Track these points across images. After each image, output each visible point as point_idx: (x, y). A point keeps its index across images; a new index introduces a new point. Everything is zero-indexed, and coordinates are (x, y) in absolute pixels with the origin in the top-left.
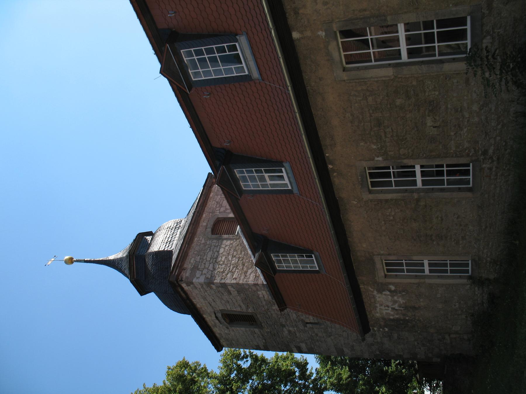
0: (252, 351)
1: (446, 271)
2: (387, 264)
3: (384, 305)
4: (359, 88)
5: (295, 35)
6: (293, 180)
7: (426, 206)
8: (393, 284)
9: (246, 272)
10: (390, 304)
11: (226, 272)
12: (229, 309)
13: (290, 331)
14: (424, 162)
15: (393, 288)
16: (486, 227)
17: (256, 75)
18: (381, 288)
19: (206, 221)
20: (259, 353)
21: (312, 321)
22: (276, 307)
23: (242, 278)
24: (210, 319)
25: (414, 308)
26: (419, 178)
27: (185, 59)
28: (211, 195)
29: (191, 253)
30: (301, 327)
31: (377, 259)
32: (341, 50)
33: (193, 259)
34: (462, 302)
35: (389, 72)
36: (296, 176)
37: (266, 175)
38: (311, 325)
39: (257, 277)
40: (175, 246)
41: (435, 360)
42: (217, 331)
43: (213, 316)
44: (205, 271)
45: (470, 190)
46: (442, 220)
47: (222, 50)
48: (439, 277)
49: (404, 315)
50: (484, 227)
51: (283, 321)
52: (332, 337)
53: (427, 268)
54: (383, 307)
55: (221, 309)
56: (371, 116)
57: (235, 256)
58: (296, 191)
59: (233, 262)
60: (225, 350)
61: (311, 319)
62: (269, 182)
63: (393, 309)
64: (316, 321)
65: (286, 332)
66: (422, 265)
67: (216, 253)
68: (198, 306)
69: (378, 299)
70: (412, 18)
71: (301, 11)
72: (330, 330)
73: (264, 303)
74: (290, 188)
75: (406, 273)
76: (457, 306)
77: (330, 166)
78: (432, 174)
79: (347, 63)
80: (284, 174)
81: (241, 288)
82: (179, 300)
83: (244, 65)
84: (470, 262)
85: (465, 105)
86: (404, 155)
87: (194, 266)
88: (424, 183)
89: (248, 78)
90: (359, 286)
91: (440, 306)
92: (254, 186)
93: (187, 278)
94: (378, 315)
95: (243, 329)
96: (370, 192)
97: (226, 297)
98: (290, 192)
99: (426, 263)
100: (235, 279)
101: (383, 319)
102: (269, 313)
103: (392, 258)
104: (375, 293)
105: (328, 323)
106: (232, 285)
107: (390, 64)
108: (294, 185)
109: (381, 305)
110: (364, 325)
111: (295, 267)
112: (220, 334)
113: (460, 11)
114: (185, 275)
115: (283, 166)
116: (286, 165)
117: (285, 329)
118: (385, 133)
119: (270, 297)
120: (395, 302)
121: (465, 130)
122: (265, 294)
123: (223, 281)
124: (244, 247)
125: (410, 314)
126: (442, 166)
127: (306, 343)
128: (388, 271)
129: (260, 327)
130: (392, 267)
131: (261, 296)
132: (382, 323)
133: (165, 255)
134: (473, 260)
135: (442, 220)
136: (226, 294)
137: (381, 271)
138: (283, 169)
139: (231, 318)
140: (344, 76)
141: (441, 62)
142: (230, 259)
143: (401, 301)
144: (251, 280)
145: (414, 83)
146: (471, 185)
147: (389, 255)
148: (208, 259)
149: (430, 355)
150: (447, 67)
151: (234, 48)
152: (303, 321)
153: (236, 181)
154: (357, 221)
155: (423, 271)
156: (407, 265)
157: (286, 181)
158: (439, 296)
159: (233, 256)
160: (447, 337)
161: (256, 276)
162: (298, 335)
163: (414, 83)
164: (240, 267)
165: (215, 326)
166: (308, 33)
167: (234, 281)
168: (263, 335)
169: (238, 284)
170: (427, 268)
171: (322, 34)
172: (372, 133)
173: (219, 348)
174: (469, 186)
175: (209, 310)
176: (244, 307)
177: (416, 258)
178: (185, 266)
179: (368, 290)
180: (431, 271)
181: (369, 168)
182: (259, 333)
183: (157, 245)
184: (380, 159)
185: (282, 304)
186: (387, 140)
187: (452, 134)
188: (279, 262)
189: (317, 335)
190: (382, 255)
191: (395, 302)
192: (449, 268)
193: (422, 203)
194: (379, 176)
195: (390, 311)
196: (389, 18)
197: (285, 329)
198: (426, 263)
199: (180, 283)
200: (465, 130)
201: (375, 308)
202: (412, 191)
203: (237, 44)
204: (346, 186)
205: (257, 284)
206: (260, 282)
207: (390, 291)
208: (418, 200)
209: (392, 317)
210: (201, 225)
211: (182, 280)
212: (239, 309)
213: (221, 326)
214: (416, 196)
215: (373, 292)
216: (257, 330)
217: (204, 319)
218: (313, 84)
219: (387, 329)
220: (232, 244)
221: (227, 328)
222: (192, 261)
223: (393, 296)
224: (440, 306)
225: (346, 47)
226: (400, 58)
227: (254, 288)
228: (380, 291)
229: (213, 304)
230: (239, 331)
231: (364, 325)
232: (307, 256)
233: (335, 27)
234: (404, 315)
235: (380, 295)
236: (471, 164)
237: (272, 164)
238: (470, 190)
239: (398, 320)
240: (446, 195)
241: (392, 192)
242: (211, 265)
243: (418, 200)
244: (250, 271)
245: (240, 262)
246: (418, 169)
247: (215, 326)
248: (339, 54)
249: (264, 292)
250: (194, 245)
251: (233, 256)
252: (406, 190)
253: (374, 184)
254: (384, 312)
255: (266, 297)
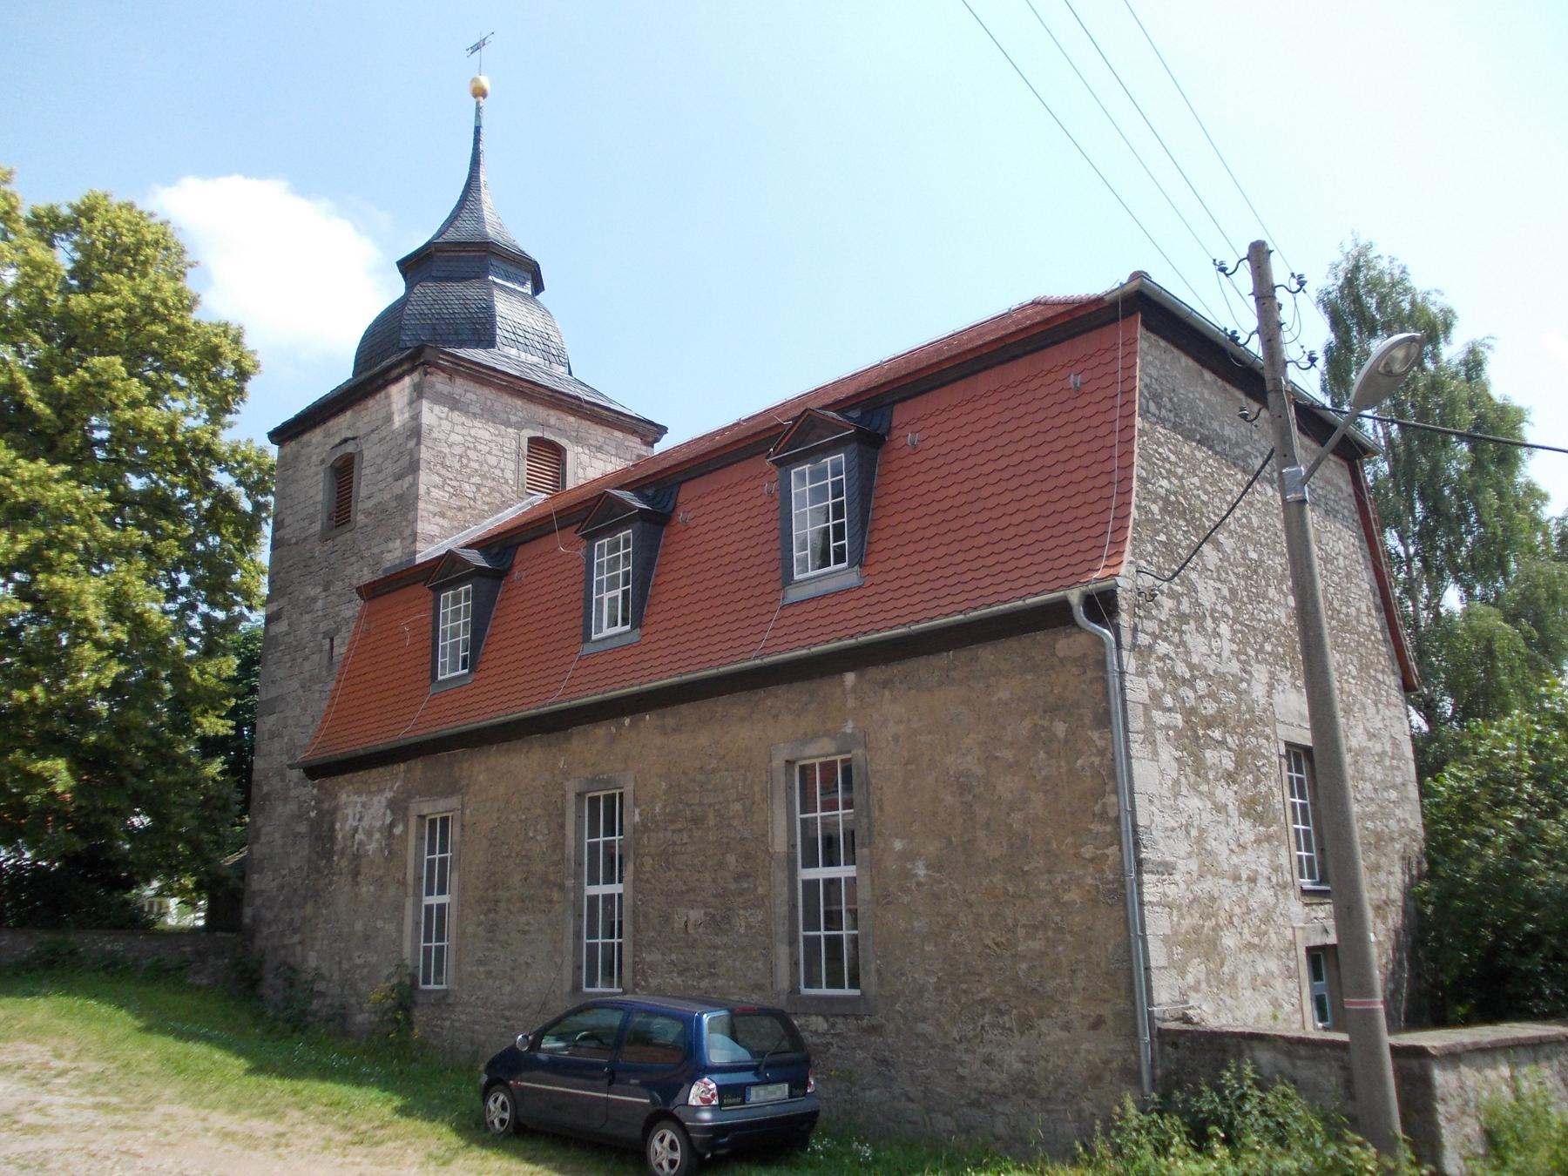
0: (270, 521)
1: (428, 939)
2: (445, 821)
3: (363, 810)
4: (756, 789)
5: (850, 678)
6: (609, 645)
7: (551, 902)
8: (406, 831)
9: (443, 516)
10: (365, 823)
11: (443, 472)
12: (364, 472)
13: (314, 600)
14: (627, 902)
15: (398, 831)
16: (507, 1019)
17: (794, 594)
18: (398, 807)
19: (556, 426)
20: (267, 530)
21: (336, 650)
22: (367, 576)
23: (431, 507)
24: (342, 425)
25: (356, 874)
26: (601, 890)
27: (828, 460)
28: (618, 434)
29: (487, 393)
30: (323, 627)
31: (454, 801)
32: (823, 760)
33: (474, 398)
34: (365, 971)
35: (780, 846)
36: (614, 649)
37: (619, 593)
38: (327, 647)
39: (431, 539)
40: (506, 357)
41: (248, 912)
42: (316, 436)
43: (350, 435)
44: (446, 425)
45: (577, 987)
46: (525, 932)
47: (839, 535)
48: (418, 924)
49: (343, 853)
50: (507, 1013)
51: (338, 586)
52: (300, 692)
53: (435, 900)
54: (359, 808)
55: (365, 453)
56: (710, 805)
57: (478, 490)
58: (588, 649)
59: (466, 486)
60: (273, 451)
61: (340, 650)
62: (606, 596)
63: (356, 830)
64: (335, 659)
65: (312, 592)
66: (442, 891)
67: (485, 449)
68: (371, 403)
69: (375, 799)
70: (864, 893)
71: (887, 693)
72: (317, 687)
73: (376, 550)
74: (594, 637)
75: (427, 857)
76: (358, 961)
77: (627, 721)
78: (607, 915)
79: (803, 768)
80: (619, 629)
81: (407, 503)
82: (392, 352)
83: (811, 574)
84: (444, 987)
85: (720, 982)
86: (642, 864)
87: (458, 401)
88: (593, 900)
89: (787, 579)
90: (404, 761)
91: (359, 926)
92: (600, 565)
93: (432, 386)
94: (343, 797)
95: (320, 497)
96: (580, 796)
97: (390, 468)
98: (587, 637)
99: (444, 899)
100: (428, 493)
101: (335, 809)
102: (354, 559)
103: (454, 832)
104: (389, 794)
105: (332, 685)
106: (415, 484)
107: (794, 846)
108: (601, 647)
109: (363, 806)
110: (323, 771)
111: (444, 632)
112: (308, 444)
113: (869, 979)
114: (439, 381)
115: (633, 628)
116: (635, 636)
117: (319, 589)
118: (680, 831)
119: (388, 565)
120: (369, 834)
121: (679, 981)
122: (393, 555)
123: (423, 465)
124: (499, 509)
125: (344, 863)
126: (620, 936)
127: (288, 634)
128: (433, 822)
129: (324, 537)
130: (439, 829)
131: (391, 545)
132: (326, 806)
133: (483, 332)
134: (446, 993)
135: (525, 932)
136: (396, 468)
137: (433, 808)
138: (628, 627)
139: (343, 472)
140: (779, 763)
141: (793, 941)
142: (473, 480)
143: (372, 847)
144: (423, 527)
145: (761, 890)
146: (585, 989)
147: (463, 826)
148: (473, 432)
149: (258, 901)
150: (783, 951)
151: (840, 558)
152: (337, 630)
153: (611, 530)
154: (524, 766)
155: (430, 893)
156: (443, 861)
157: (606, 630)
158: (380, 924)
159: (479, 487)
160: (296, 938)
161: (433, 537)
162: (307, 617)
163: (761, 890)
164: (455, 502)
165: (328, 435)
166: (851, 703)
167: (422, 489)
168: (305, 539)
169: (417, 498)
170: (435, 900)
171: (849, 728)
172: (680, 806)
173: (280, 435)
174: (802, 987)
175: (362, 427)
176: (369, 504)
177: (453, 879)
178: (459, 381)
179: (393, 780)
180: (429, 908)
181: (621, 795)
182: (311, 531)
183: (509, 309)
184: (637, 818)
185: (370, 592)
186: (669, 834)
187: (674, 957)
188: (456, 600)
189: (306, 659)
190: (463, 813)
191: (369, 834)
192: (434, 944)
193: (556, 895)
194: (606, 811)
195: (351, 823)
196: (865, 851)
197: (319, 589)
198: (444, 899)
199: (421, 370)
200: (679, 981)
201: (359, 793)
202: (578, 876)
203: (845, 565)
204: (590, 750)
205: (415, 541)
206: (420, 546)
207: (392, 825)
208: (561, 887)
209: (338, 826)
210: (552, 412)
211: (426, 373)
212: (363, 493)
213: (328, 448)
214: (569, 883)
215: (391, 789)
216: (317, 527)
217: (342, 410)
218: (769, 702)
219: (313, 814)
220: (506, 482)
221: (323, 462)
222: (469, 395)
223: (380, 830)
224: (359, 926)
225: (829, 768)
226: (805, 865)
227: (407, 532)
228: (393, 805)
229: (375, 437)
230: (315, 488)
231: (323, 771)
232: (465, 658)
233: (858, 753)
234: (343, 853)
235: (384, 803)
236: (856, 992)
237: (637, 608)
238: (577, 987)
239: (332, 838)
240: (569, 943)
241: (577, 836)
242: (459, 439)
243: (561, 887)
244: (445, 523)
245: (464, 503)
246: (616, 889)
247: (328, 435)
248: (817, 752)
249: (398, 553)
250: (508, 400)
251: (479, 487)
252: (580, 865)
253: (594, 802)
254: (350, 811)
255: (388, 556)
